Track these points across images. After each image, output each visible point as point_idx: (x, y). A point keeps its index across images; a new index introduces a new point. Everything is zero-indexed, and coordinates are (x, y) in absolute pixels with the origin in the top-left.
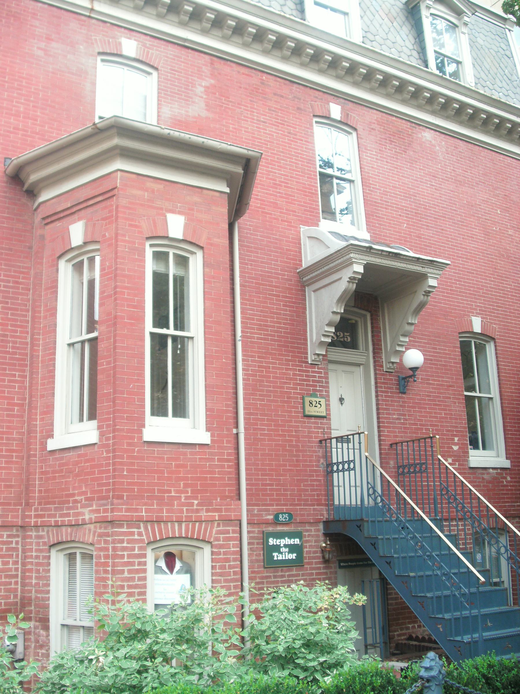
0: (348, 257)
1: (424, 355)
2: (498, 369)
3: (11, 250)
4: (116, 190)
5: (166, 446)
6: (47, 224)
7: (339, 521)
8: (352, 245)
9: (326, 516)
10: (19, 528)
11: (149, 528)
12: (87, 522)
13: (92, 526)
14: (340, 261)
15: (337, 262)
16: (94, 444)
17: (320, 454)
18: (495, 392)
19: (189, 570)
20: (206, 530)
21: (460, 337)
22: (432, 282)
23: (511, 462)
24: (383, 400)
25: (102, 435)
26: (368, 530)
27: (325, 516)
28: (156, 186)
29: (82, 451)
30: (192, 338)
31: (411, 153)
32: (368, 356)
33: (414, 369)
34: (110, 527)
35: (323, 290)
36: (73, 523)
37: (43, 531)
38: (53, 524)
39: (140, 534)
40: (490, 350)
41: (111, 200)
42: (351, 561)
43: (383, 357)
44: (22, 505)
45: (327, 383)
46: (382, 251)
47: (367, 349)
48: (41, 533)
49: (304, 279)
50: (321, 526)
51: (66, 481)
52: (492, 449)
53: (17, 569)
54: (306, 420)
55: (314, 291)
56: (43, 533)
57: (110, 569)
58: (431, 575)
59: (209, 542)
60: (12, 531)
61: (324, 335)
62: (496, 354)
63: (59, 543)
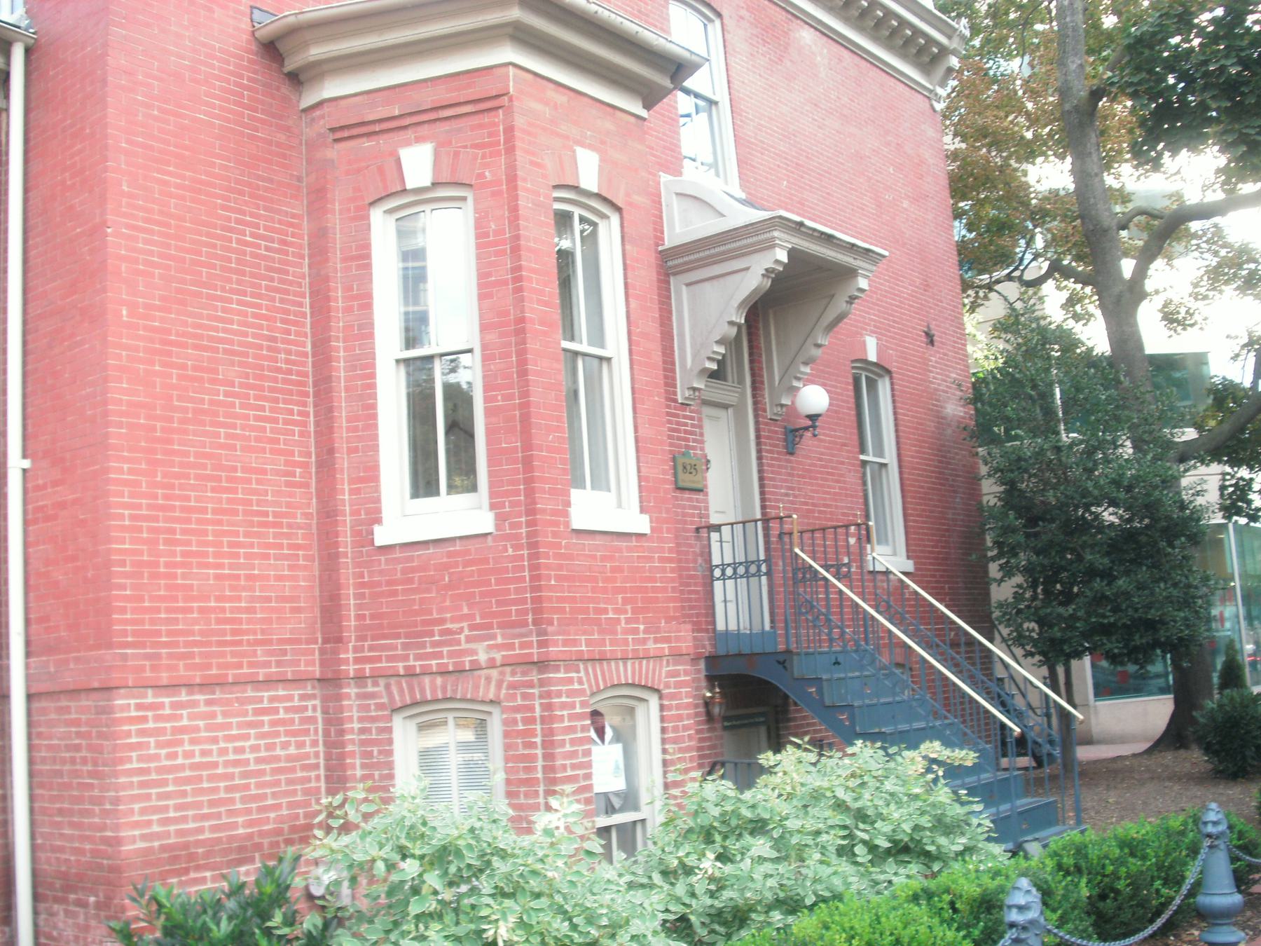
0: (767, 236)
1: (831, 398)
2: (896, 419)
3: (271, 181)
4: (506, 98)
5: (598, 537)
6: (336, 140)
7: (740, 655)
8: (780, 217)
9: (709, 649)
10: (316, 683)
11: (590, 671)
12: (483, 664)
13: (494, 673)
14: (750, 241)
15: (745, 242)
16: (640, 536)
17: (698, 550)
18: (890, 457)
19: (625, 738)
20: (654, 670)
21: (854, 368)
22: (863, 283)
23: (915, 564)
24: (769, 465)
25: (500, 519)
26: (799, 668)
27: (708, 649)
28: (561, 98)
29: (458, 547)
30: (609, 360)
31: (789, 64)
32: (743, 394)
33: (813, 417)
34: (535, 672)
35: (707, 285)
36: (451, 668)
37: (376, 684)
38: (402, 672)
39: (580, 682)
40: (884, 388)
41: (493, 113)
42: (738, 717)
43: (767, 396)
44: (316, 643)
45: (702, 435)
46: (815, 230)
47: (741, 381)
48: (370, 689)
49: (670, 263)
50: (702, 665)
51: (421, 599)
52: (887, 542)
53: (317, 755)
54: (678, 494)
55: (688, 285)
56: (376, 689)
57: (538, 740)
58: (908, 731)
59: (658, 691)
60: (305, 688)
61: (709, 359)
62: (893, 396)
63: (415, 704)
